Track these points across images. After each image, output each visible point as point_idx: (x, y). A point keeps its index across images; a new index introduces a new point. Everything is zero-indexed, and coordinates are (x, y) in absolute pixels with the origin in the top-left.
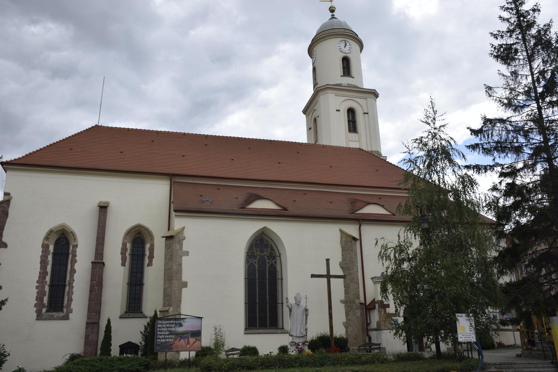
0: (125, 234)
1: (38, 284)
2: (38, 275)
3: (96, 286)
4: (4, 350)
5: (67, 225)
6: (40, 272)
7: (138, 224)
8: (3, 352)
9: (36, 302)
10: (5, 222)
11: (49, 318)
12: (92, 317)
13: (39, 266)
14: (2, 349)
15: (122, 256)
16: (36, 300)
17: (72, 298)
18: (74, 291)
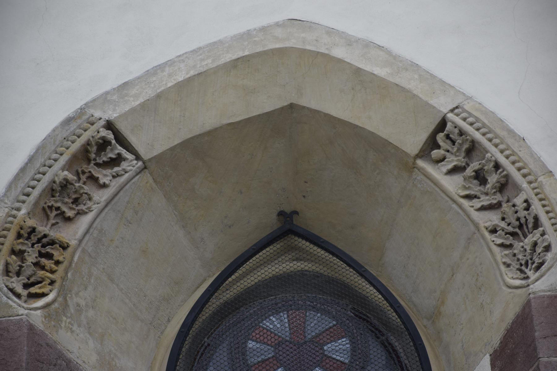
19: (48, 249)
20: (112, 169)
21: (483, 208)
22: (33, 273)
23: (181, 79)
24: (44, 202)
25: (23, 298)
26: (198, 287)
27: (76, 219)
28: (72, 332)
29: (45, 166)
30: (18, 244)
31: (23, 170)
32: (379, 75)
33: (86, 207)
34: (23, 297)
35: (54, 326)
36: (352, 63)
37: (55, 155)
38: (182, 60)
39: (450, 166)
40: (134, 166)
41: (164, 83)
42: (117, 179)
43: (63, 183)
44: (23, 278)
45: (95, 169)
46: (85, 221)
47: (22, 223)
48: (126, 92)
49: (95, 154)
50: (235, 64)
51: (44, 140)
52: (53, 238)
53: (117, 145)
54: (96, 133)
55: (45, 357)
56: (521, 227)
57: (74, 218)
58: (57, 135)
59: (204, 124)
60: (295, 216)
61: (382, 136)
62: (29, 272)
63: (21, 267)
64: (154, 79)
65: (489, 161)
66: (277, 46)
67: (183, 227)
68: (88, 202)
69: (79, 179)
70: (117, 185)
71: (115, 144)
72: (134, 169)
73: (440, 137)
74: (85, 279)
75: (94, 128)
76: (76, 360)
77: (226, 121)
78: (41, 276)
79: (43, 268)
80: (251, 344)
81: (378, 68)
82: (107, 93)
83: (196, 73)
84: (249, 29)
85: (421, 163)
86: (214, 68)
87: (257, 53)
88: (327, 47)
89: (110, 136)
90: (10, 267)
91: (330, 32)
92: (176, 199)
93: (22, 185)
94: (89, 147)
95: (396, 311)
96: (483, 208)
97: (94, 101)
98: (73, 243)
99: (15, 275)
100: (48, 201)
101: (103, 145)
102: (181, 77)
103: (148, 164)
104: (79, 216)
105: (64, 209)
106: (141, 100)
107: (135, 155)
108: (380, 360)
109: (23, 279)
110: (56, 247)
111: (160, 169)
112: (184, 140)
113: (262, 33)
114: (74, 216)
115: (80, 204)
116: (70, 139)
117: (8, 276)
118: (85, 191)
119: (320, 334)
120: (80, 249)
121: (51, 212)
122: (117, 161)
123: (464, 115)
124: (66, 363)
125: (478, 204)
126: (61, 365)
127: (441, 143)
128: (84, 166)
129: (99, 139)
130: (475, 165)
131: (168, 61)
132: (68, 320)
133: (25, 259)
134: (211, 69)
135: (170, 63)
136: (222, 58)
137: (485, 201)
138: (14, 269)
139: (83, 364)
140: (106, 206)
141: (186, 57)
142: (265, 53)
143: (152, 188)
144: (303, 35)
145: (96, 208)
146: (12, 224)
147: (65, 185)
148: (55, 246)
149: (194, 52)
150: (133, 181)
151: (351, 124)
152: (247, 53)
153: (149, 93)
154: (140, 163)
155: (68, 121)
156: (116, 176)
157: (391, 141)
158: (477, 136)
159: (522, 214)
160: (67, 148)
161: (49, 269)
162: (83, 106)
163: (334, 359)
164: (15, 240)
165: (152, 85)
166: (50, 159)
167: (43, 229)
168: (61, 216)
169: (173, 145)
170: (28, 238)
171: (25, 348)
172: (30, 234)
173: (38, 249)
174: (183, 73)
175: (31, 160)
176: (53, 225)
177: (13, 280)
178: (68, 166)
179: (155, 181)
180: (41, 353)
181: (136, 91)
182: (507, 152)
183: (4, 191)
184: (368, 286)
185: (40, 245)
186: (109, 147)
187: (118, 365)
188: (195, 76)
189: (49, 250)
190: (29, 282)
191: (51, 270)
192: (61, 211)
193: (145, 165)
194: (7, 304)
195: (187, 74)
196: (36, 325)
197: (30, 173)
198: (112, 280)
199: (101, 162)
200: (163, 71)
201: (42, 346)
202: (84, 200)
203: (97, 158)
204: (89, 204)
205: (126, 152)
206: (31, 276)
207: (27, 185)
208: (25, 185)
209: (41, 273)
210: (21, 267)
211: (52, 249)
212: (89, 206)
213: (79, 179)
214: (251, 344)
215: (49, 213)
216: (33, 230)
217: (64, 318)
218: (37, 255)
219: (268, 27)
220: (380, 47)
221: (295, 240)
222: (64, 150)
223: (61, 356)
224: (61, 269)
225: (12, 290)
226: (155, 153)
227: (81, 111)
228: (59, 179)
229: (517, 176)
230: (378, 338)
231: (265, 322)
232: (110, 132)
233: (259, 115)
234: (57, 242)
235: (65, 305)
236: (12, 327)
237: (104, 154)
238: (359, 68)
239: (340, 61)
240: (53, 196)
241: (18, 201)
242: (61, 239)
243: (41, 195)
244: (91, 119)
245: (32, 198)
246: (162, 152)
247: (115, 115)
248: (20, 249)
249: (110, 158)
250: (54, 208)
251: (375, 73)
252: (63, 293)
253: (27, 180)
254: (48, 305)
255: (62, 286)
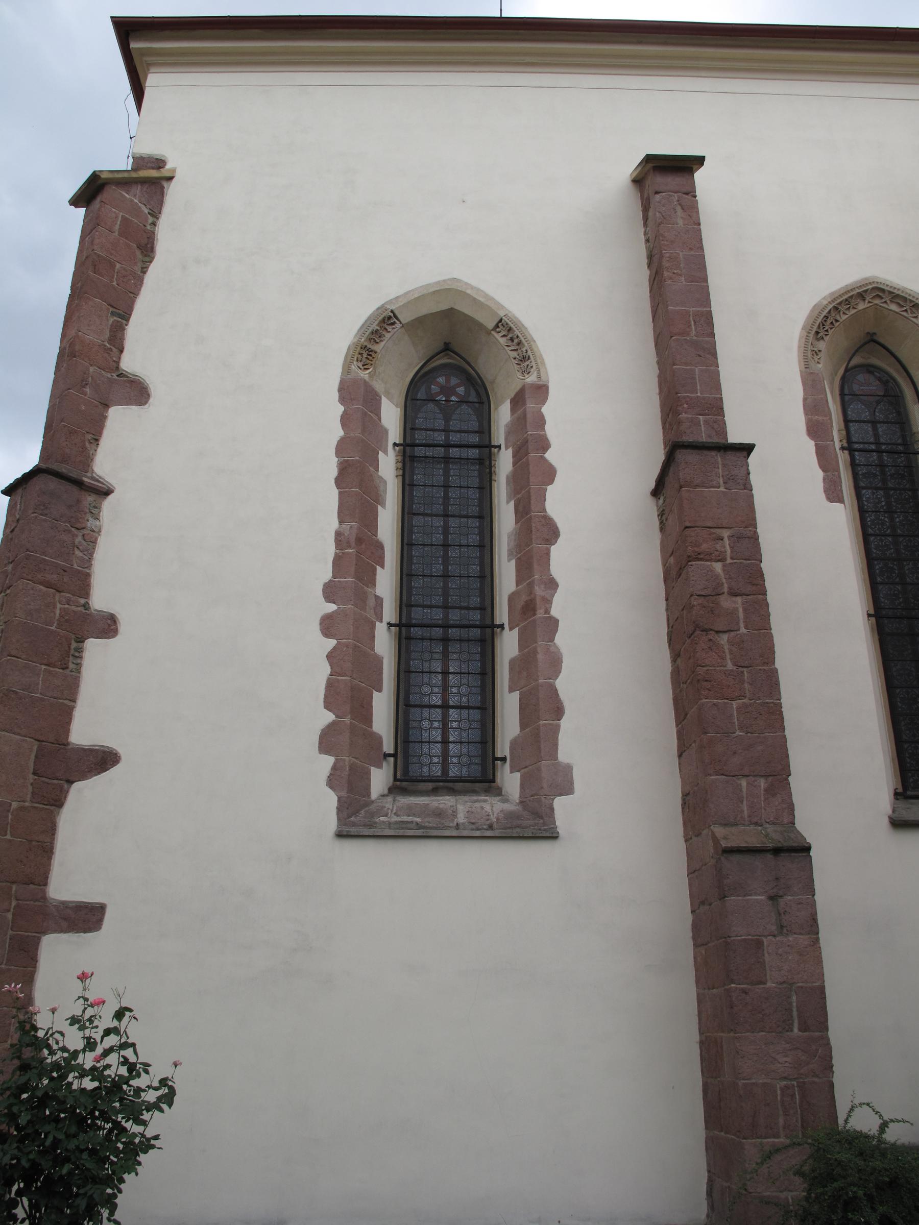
0: (807, 328)
1: (332, 607)
2: (331, 549)
3: (733, 594)
4: (129, 1053)
5: (472, 288)
6: (338, 534)
7: (867, 282)
8: (123, 1071)
9: (330, 717)
10: (140, 282)
11: (419, 826)
12: (745, 807)
13: (331, 497)
14: (112, 1040)
15: (817, 446)
16: (328, 705)
17: (554, 693)
18: (564, 650)
19: (370, 353)
21: (512, 350)
39: (502, 334)
50: (434, 292)
56: (524, 358)
62: (365, 361)
65: (515, 335)
73: (500, 324)
79: (368, 359)
80: (433, 386)
82: (391, 300)
85: (492, 332)
89: (392, 315)
96: (512, 350)
98: (378, 351)
101: (390, 318)
102: (416, 296)
105: (376, 339)
109: (362, 363)
123: (508, 318)
125: (510, 348)
127: (500, 326)
130: (510, 335)
135: (413, 290)
136: (869, 1218)
137: (513, 348)
145: (386, 339)
147: (377, 331)
154: (401, 325)
155: (378, 309)
156: (393, 329)
158: (512, 326)
159: (525, 354)
167: (369, 346)
172: (365, 347)
178: (378, 325)
179: (406, 331)
182: (521, 332)
197: (365, 326)
204: (384, 338)
216: (366, 346)
223: (373, 389)
224: (374, 359)
225: (358, 367)
226: (406, 322)
227: (383, 306)
229: (524, 341)
235: (375, 372)
241: (362, 336)
243: (369, 334)
252: (374, 369)
254: (370, 373)
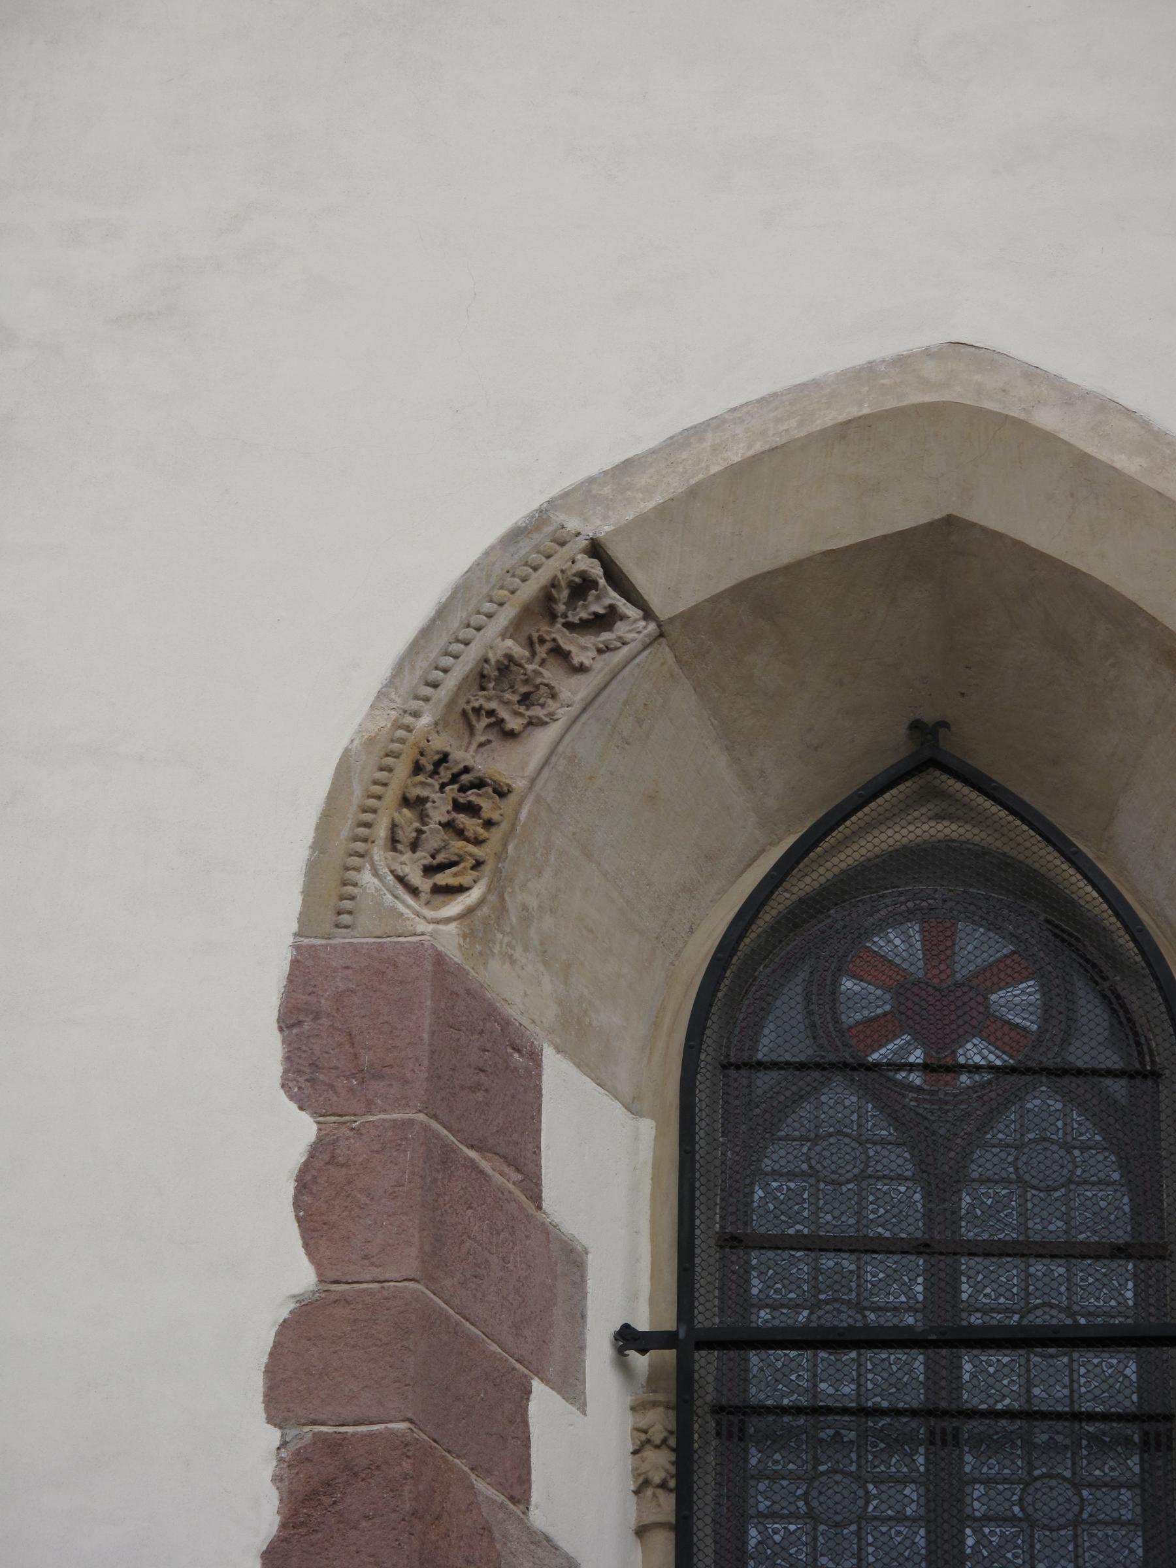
19: (472, 796)
20: (597, 634)
22: (443, 844)
23: (736, 459)
24: (465, 700)
25: (424, 896)
26: (749, 865)
27: (525, 735)
28: (513, 962)
29: (468, 626)
30: (415, 785)
31: (426, 633)
32: (1125, 471)
33: (545, 712)
34: (422, 894)
35: (481, 954)
36: (1072, 442)
37: (488, 604)
38: (739, 418)
40: (639, 632)
41: (703, 465)
42: (606, 656)
43: (502, 663)
44: (424, 854)
45: (564, 633)
46: (544, 738)
47: (423, 743)
48: (628, 479)
49: (564, 604)
50: (843, 431)
51: (467, 572)
52: (480, 774)
53: (609, 588)
54: (570, 563)
55: (465, 1018)
57: (520, 733)
58: (494, 564)
59: (778, 551)
60: (942, 731)
61: (1126, 595)
63: (420, 832)
64: (684, 455)
66: (927, 399)
67: (727, 749)
68: (550, 702)
69: (534, 653)
70: (606, 670)
71: (605, 587)
72: (640, 637)
74: (538, 855)
75: (565, 552)
76: (519, 1018)
77: (820, 547)
78: (457, 851)
79: (460, 833)
80: (848, 984)
81: (1123, 457)
82: (591, 480)
83: (767, 447)
84: (871, 359)
86: (802, 437)
87: (886, 411)
88: (1023, 406)
89: (596, 570)
90: (400, 832)
91: (1032, 374)
92: (716, 695)
93: (425, 664)
94: (554, 592)
95: (1134, 940)
97: (566, 495)
98: (519, 784)
99: (408, 848)
100: (473, 698)
101: (582, 587)
103: (667, 628)
104: (530, 728)
105: (504, 713)
106: (658, 499)
107: (642, 610)
108: (1099, 1030)
110: (487, 792)
111: (690, 638)
112: (737, 582)
113: (897, 370)
114: (521, 728)
115: (533, 705)
116: (518, 572)
117: (395, 849)
118: (546, 681)
119: (984, 970)
120: (531, 798)
121: (479, 719)
122: (606, 620)
124: (502, 1026)
126: (492, 1032)
128: (545, 628)
129: (574, 575)
131: (713, 418)
132: (506, 940)
133: (428, 816)
134: (796, 440)
135: (715, 424)
138: (407, 837)
139: (531, 1027)
140: (584, 710)
141: (748, 413)
142: (902, 412)
143: (672, 675)
144: (978, 378)
145: (564, 715)
146: (404, 743)
147: (507, 665)
148: (484, 790)
149: (763, 401)
150: (638, 660)
151: (1065, 565)
152: (866, 411)
153: (673, 485)
154: (652, 626)
155: (515, 535)
157: (1142, 605)
160: (513, 592)
161: (473, 836)
162: (545, 505)
163: (1008, 1022)
164: (410, 777)
165: (680, 469)
166: (479, 613)
167: (462, 756)
168: (496, 729)
169: (718, 591)
170: (435, 773)
171: (429, 1003)
173: (453, 795)
174: (742, 445)
175: (442, 612)
176: (481, 745)
177: (404, 858)
178: (514, 629)
179: (678, 661)
180: (456, 1011)
181: (649, 480)
183: (388, 674)
184: (1081, 884)
185: (456, 786)
186: (593, 592)
187: (595, 1023)
188: (763, 453)
189: (473, 798)
190: (435, 862)
191: (476, 838)
192: (497, 717)
193: (661, 631)
194: (393, 909)
195: (749, 448)
196: (448, 953)
197: (440, 641)
198: (589, 856)
199: (576, 620)
200: (701, 440)
201: (458, 995)
202: (541, 696)
203: (570, 613)
204: (552, 705)
205: (624, 604)
206: (438, 851)
207: (434, 665)
208: (431, 664)
209: (458, 845)
210: (420, 832)
211: (479, 795)
212: (551, 710)
213: (534, 653)
214: (848, 984)
215: (474, 722)
216: (444, 758)
217: (499, 936)
218: (450, 808)
219: (909, 356)
220: (1128, 413)
221: (935, 778)
222: (505, 596)
223: (492, 1013)
224: (495, 835)
225: (401, 879)
227: (540, 518)
228: (496, 654)
230: (1097, 983)
231: (876, 939)
232: (596, 562)
233: (885, 537)
234: (490, 782)
235: (502, 909)
236: (403, 958)
237: (583, 605)
238: (1086, 454)
239: (1047, 437)
240: (483, 689)
241: (416, 698)
242: (497, 777)
243: (460, 688)
244: (558, 534)
245: (443, 693)
246: (696, 606)
247: (607, 528)
248: (418, 796)
249: (595, 613)
250: (483, 712)
251: (1118, 466)
252: (498, 887)
253: (433, 655)
254: (469, 912)
255: (497, 871)
